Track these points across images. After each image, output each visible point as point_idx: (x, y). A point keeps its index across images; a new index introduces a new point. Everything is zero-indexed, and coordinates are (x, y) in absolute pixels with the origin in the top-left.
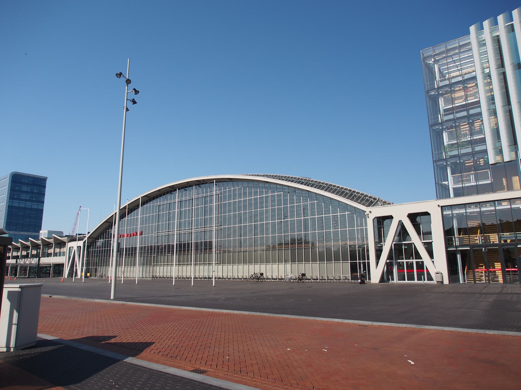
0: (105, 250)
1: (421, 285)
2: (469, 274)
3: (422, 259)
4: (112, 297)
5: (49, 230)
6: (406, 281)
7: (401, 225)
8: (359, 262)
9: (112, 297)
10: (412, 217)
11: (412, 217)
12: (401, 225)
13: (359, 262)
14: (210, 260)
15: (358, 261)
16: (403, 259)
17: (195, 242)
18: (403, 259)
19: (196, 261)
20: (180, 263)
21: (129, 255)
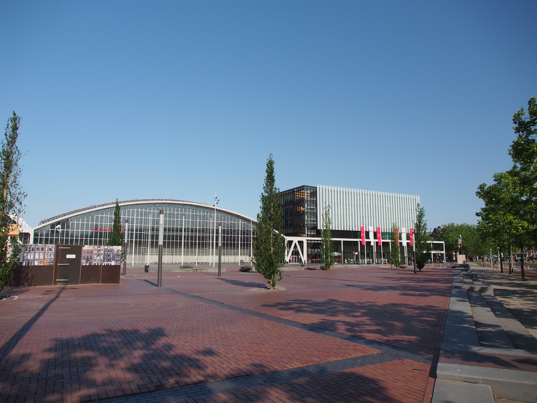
0: (145, 241)
1: (295, 264)
2: (363, 262)
3: (369, 239)
4: (214, 267)
5: (494, 288)
6: (294, 263)
7: (295, 244)
8: (140, 218)
9: (214, 267)
10: (299, 242)
11: (299, 242)
12: (295, 244)
13: (138, 217)
14: (180, 252)
15: (104, 223)
16: (343, 241)
17: (223, 228)
18: (343, 241)
19: (184, 253)
20: (186, 254)
21: (244, 247)
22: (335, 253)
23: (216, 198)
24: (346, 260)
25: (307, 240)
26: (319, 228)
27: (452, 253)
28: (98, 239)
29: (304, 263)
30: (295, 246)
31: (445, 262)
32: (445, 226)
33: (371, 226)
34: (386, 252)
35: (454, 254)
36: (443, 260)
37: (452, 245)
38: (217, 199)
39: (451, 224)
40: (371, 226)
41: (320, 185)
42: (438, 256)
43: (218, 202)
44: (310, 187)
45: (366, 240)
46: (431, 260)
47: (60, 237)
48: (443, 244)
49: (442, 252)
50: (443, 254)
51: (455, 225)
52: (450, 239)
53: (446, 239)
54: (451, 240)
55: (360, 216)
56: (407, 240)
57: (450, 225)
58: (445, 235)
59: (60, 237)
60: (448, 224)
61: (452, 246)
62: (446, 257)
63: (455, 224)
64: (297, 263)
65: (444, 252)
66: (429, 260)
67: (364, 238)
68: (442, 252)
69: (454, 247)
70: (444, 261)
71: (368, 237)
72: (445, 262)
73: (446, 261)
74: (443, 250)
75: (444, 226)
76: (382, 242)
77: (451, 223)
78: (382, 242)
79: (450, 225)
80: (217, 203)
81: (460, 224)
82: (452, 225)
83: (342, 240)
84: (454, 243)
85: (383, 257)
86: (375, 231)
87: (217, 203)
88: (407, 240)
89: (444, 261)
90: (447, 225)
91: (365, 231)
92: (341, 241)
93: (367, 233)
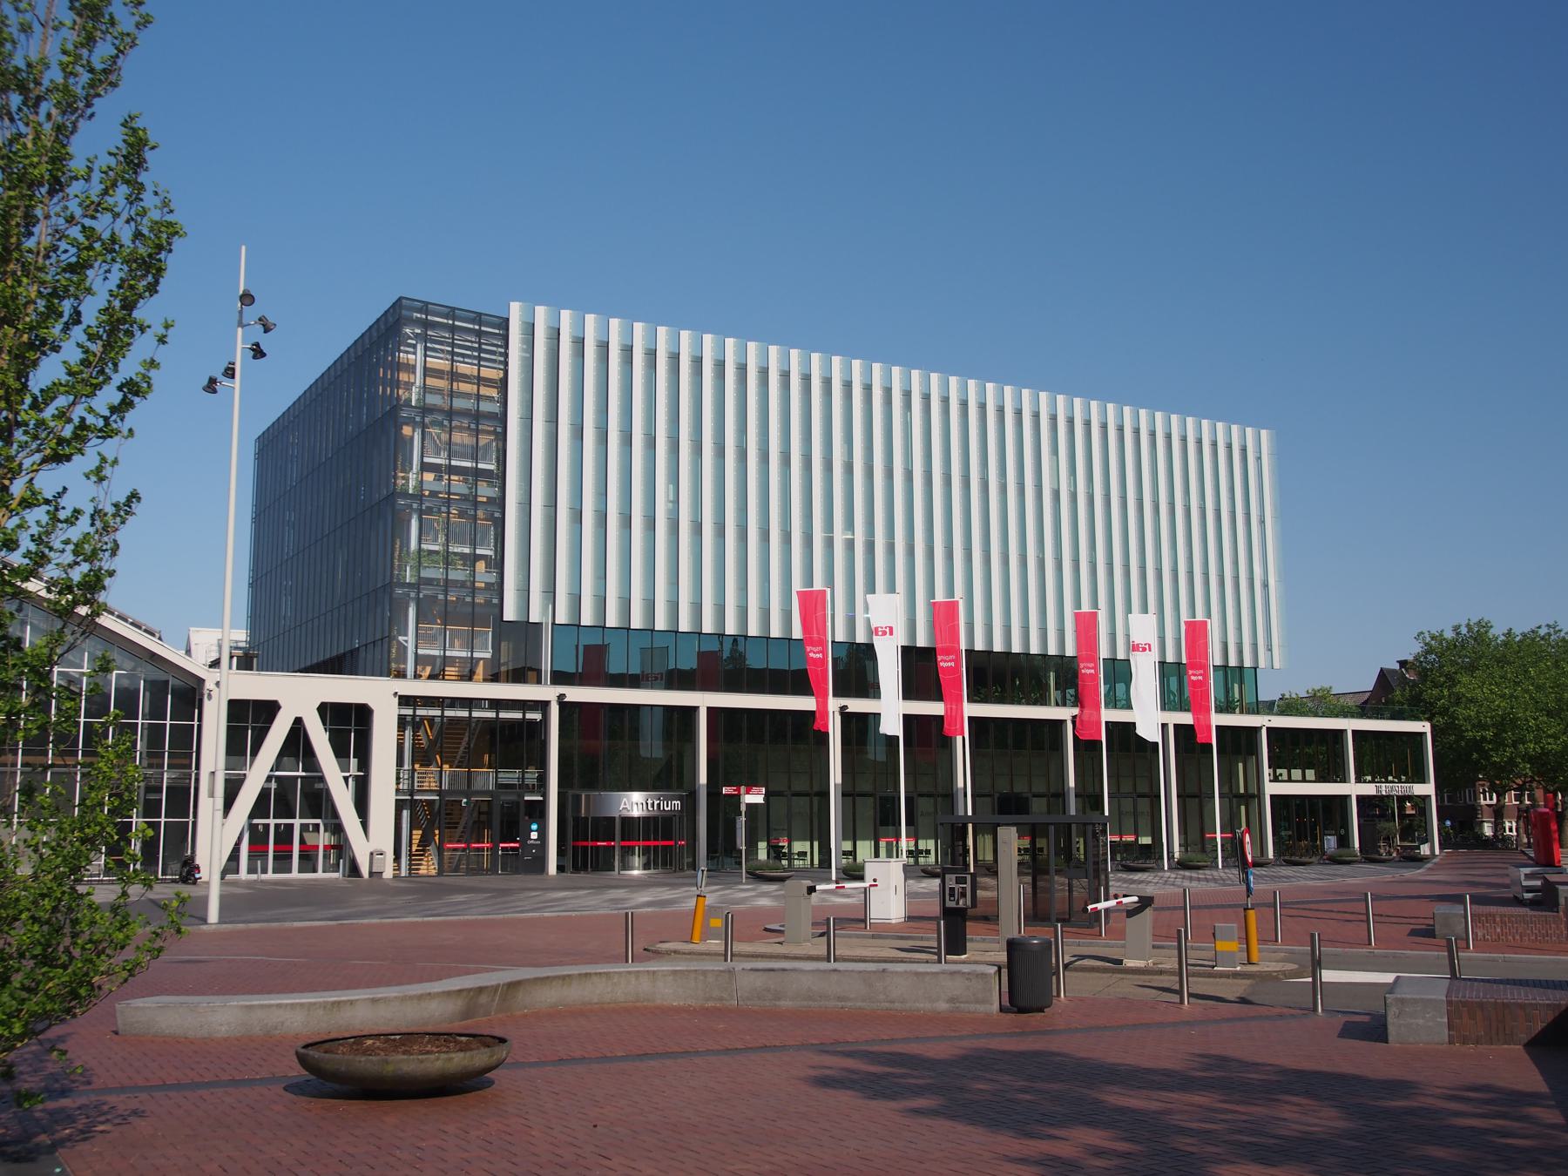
10: (326, 710)
11: (326, 710)
22: (637, 797)
23: (247, 298)
24: (762, 845)
25: (405, 701)
26: (510, 614)
27: (1476, 798)
28: (168, 722)
29: (365, 871)
30: (297, 740)
31: (1437, 851)
32: (1433, 638)
33: (1146, 611)
34: (1034, 790)
35: (1483, 802)
36: (1425, 841)
37: (1477, 745)
38: (251, 313)
39: (1468, 625)
40: (1146, 611)
41: (531, 300)
42: (1402, 816)
43: (257, 334)
44: (452, 312)
45: (1108, 715)
46: (1344, 841)
47: (805, 703)
48: (1422, 735)
49: (1419, 789)
50: (1426, 798)
51: (1498, 631)
52: (1461, 712)
53: (1444, 711)
54: (1467, 719)
55: (850, 545)
56: (1163, 708)
57: (1464, 630)
58: (1435, 692)
59: (805, 703)
60: (1456, 629)
61: (1475, 756)
62: (1441, 819)
63: (1492, 632)
64: (320, 875)
65: (1427, 789)
66: (1331, 842)
67: (962, 701)
68: (1419, 789)
69: (1488, 758)
70: (1431, 848)
71: (867, 686)
72: (1437, 851)
73: (1441, 848)
74: (1422, 779)
75: (1428, 639)
76: (970, 718)
77: (1474, 620)
78: (970, 718)
79: (1464, 630)
80: (258, 352)
81: (1521, 628)
82: (1479, 634)
83: (703, 700)
84: (1489, 734)
85: (907, 824)
86: (922, 641)
87: (258, 352)
88: (1163, 708)
89: (1431, 848)
90: (1449, 635)
91: (963, 646)
92: (695, 709)
93: (1119, 672)
